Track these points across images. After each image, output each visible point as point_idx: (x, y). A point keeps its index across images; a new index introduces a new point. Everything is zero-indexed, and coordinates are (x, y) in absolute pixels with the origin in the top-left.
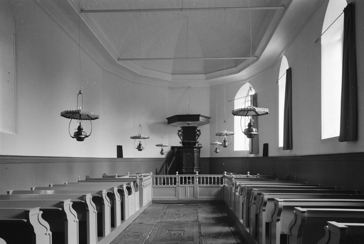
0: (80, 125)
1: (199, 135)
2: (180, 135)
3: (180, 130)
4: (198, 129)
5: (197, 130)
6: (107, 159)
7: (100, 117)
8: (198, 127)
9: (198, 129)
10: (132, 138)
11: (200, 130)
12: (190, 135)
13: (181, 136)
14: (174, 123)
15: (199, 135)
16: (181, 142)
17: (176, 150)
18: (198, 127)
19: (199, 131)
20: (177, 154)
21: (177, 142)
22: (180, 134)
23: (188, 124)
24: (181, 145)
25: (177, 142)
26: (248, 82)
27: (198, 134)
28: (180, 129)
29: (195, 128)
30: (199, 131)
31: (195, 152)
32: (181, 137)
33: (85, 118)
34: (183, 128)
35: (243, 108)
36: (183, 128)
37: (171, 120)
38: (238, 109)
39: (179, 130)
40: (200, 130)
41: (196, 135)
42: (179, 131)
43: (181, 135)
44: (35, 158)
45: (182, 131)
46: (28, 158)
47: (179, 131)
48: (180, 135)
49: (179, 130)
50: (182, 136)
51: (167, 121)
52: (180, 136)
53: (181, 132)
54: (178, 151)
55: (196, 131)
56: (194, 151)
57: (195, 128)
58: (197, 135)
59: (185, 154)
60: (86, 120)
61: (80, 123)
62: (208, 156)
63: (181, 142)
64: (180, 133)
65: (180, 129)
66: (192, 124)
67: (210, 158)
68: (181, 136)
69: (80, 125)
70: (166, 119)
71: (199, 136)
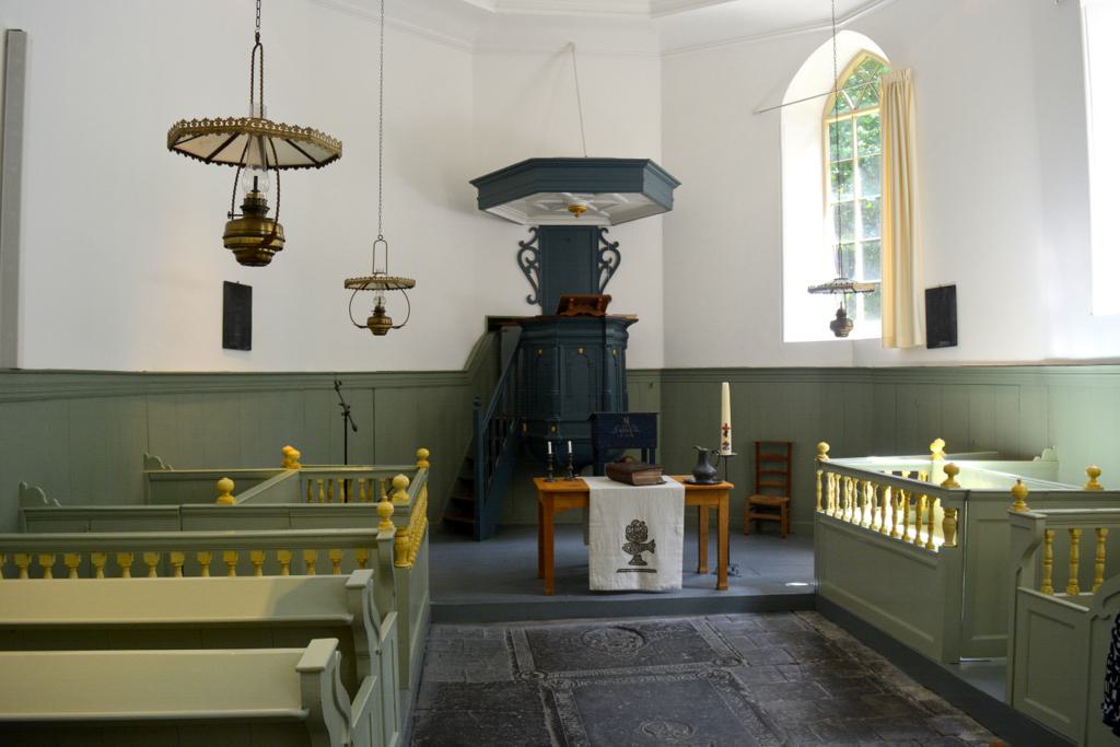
0: (255, 190)
1: (612, 265)
2: (526, 264)
3: (526, 241)
4: (610, 237)
5: (604, 241)
6: (419, 376)
7: (345, 152)
8: (607, 231)
9: (610, 237)
10: (812, 290)
11: (617, 244)
12: (570, 266)
13: (532, 270)
14: (503, 207)
15: (612, 265)
16: (533, 298)
17: (512, 335)
18: (607, 231)
19: (614, 247)
20: (521, 351)
21: (517, 298)
22: (527, 260)
23: (575, 210)
24: (535, 311)
25: (517, 298)
26: (847, 28)
27: (611, 260)
28: (528, 237)
29: (595, 233)
30: (614, 247)
31: (609, 342)
32: (533, 275)
33: (197, 154)
34: (543, 233)
35: (237, 116)
36: (543, 233)
37: (497, 188)
38: (189, 119)
39: (521, 243)
40: (617, 244)
41: (600, 265)
42: (524, 246)
43: (531, 264)
44: (386, 376)
45: (535, 245)
46: (107, 379)
47: (524, 246)
48: (526, 264)
49: (521, 243)
50: (537, 271)
51: (475, 191)
52: (526, 271)
53: (533, 249)
54: (523, 342)
55: (601, 246)
56: (604, 337)
57: (595, 233)
58: (606, 264)
59: (562, 350)
60: (296, 167)
61: (256, 178)
62: (656, 361)
63: (533, 298)
64: (529, 255)
65: (528, 237)
66: (589, 208)
67: (664, 372)
68: (532, 270)
69: (255, 190)
70: (471, 186)
71: (612, 271)
